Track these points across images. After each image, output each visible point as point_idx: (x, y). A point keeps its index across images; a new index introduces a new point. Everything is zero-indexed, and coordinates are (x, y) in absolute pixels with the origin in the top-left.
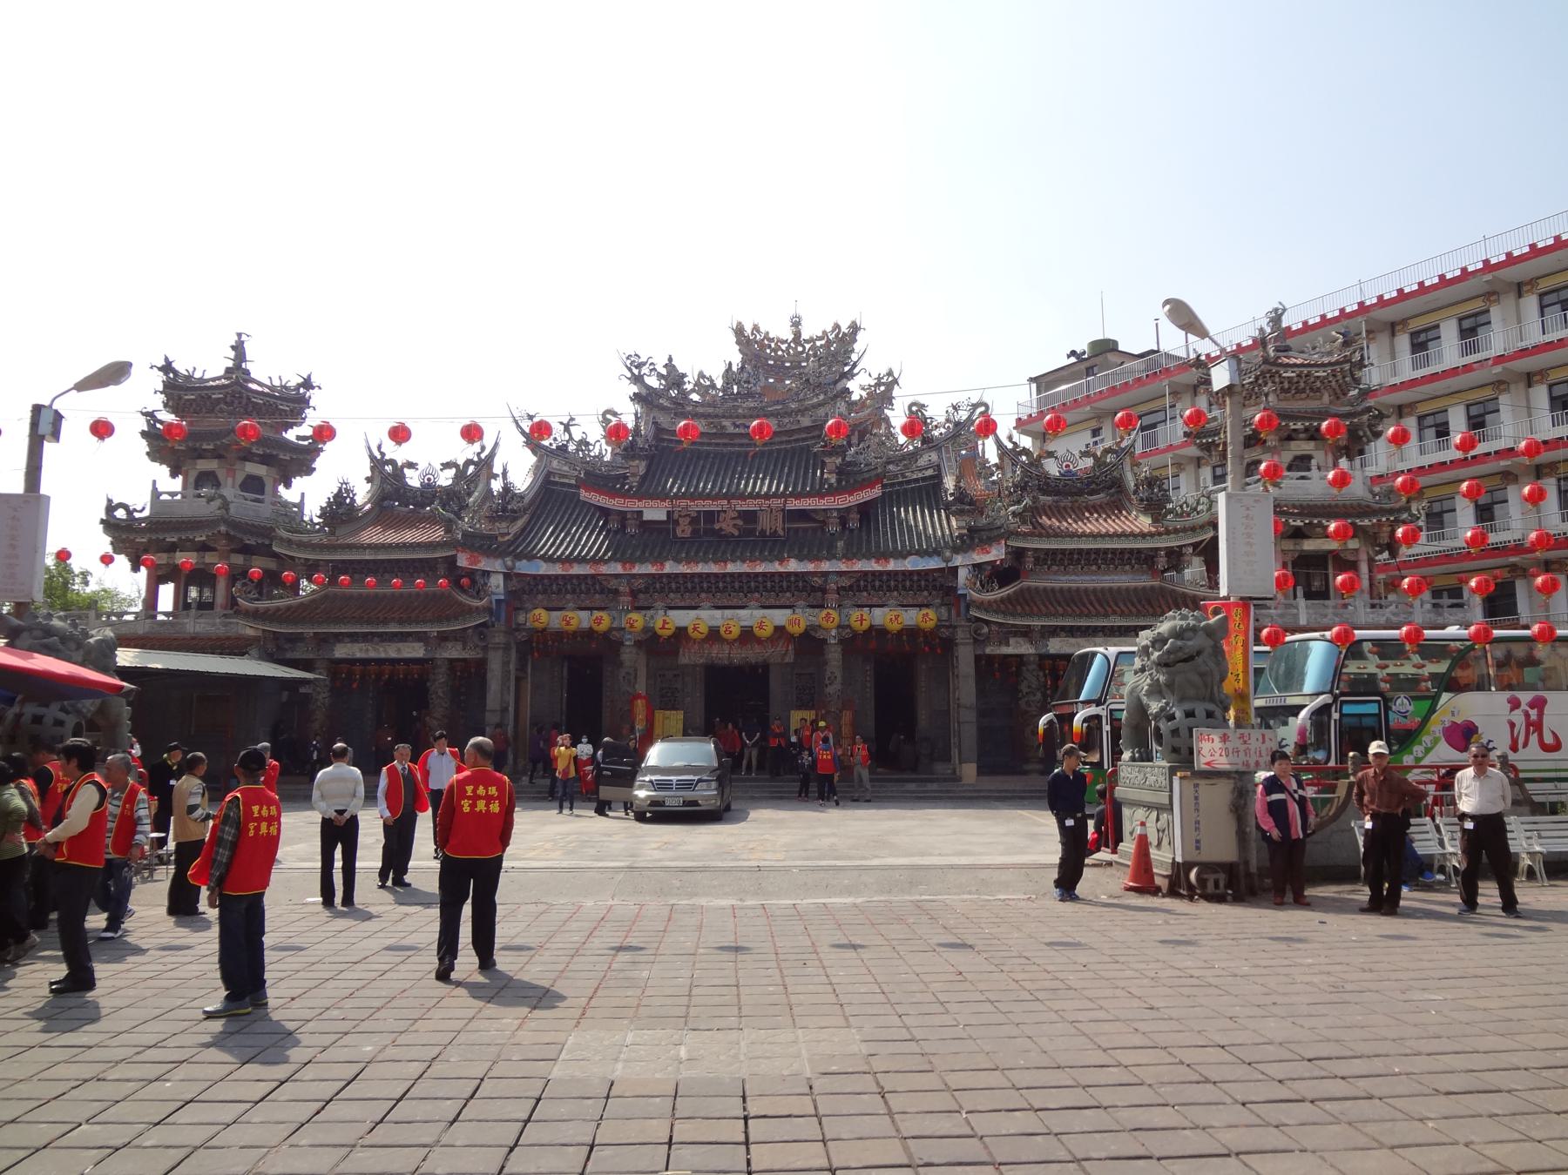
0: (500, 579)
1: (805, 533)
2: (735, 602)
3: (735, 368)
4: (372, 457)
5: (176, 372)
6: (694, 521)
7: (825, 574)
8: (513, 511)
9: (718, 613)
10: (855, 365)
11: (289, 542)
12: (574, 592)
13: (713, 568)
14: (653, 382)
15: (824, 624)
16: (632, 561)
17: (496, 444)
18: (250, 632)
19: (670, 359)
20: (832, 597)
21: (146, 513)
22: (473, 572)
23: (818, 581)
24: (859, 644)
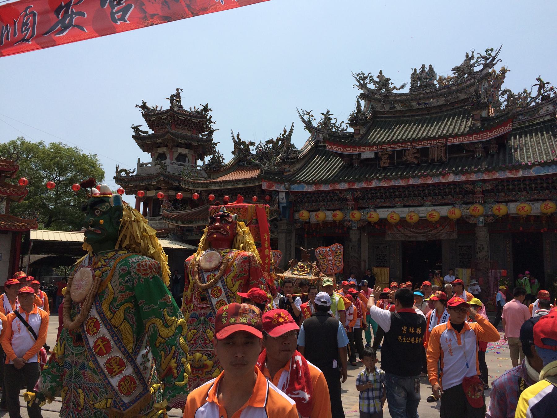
0: (284, 194)
1: (457, 154)
2: (416, 203)
3: (418, 72)
4: (235, 142)
5: (148, 108)
6: (391, 157)
7: (474, 182)
8: (291, 159)
9: (406, 210)
10: (494, 59)
11: (188, 182)
12: (324, 200)
13: (401, 183)
14: (371, 86)
15: (474, 213)
16: (354, 181)
17: (292, 130)
18: (170, 226)
19: (381, 72)
20: (479, 197)
21: (135, 173)
22: (271, 192)
23: (469, 187)
24: (499, 226)
